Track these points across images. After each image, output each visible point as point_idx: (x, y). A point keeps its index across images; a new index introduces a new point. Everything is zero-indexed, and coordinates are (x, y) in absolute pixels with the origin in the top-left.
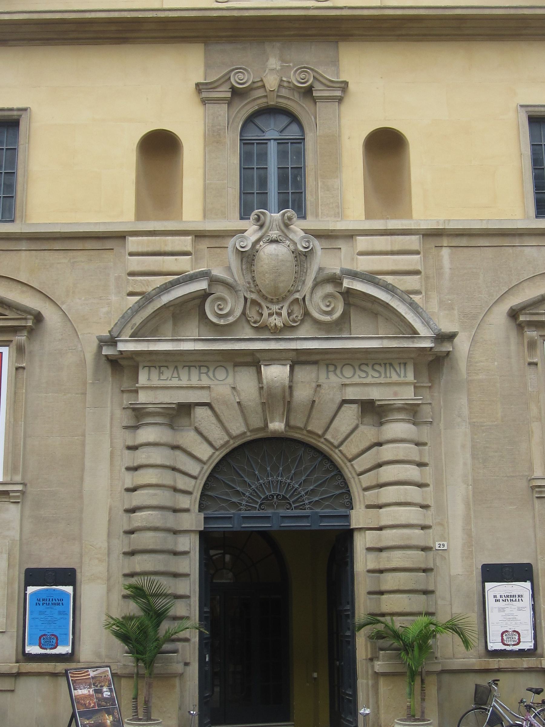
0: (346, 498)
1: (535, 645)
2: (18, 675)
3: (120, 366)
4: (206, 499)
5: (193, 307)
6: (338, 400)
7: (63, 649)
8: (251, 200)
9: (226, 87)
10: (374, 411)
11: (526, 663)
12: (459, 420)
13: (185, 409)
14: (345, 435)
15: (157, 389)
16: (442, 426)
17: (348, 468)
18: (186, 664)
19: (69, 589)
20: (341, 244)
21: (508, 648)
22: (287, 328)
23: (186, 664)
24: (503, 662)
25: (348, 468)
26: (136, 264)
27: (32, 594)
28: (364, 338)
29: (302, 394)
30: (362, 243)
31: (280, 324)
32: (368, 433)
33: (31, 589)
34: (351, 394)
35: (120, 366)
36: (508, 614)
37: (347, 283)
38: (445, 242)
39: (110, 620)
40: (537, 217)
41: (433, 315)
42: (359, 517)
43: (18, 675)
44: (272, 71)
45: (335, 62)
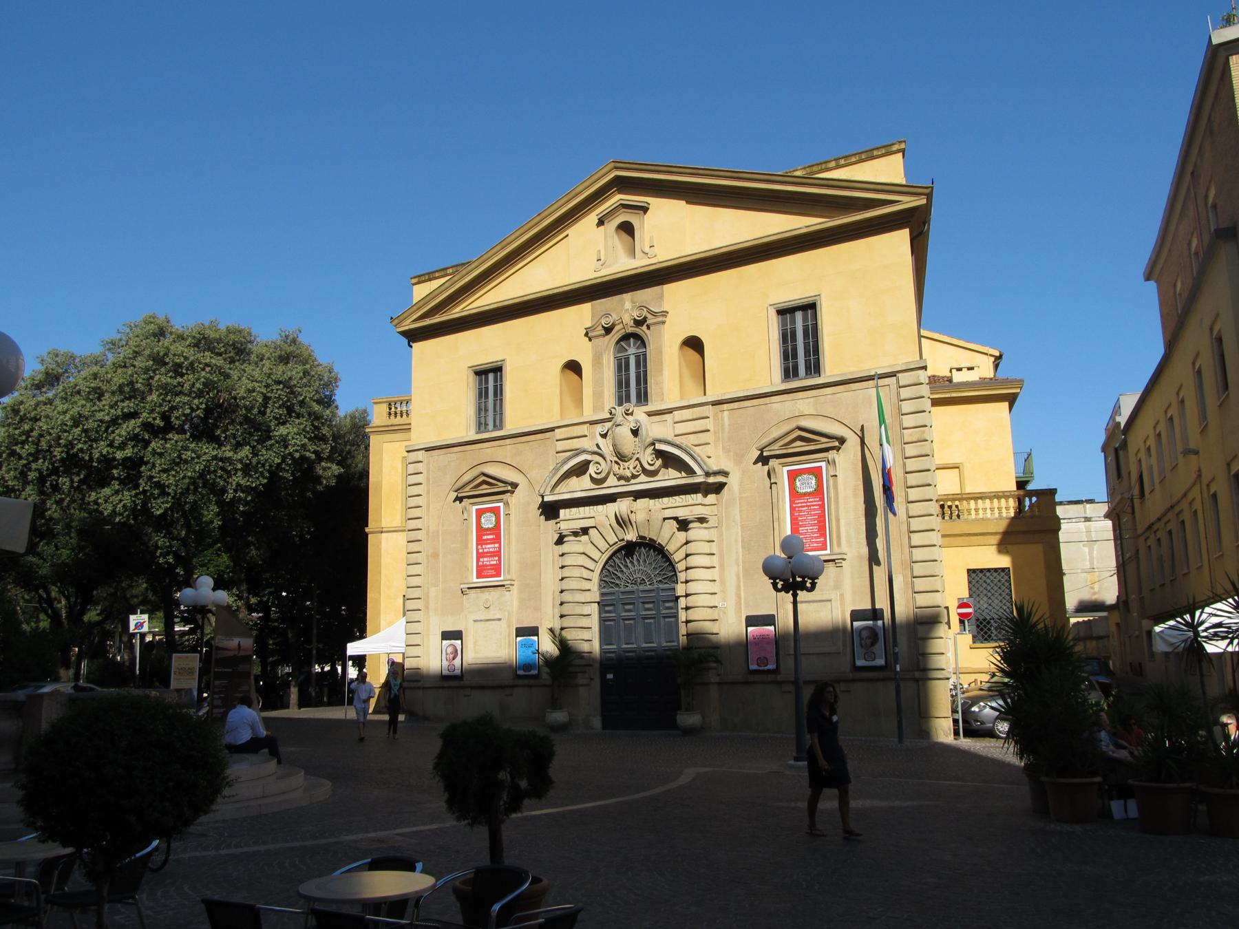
0: (674, 578)
2: (513, 686)
3: (550, 510)
4: (604, 582)
5: (581, 469)
7: (771, 667)
8: (623, 398)
10: (683, 525)
11: (770, 677)
15: (570, 518)
19: (535, 638)
20: (667, 417)
22: (634, 477)
24: (757, 678)
26: (561, 446)
28: (671, 477)
30: (678, 415)
32: (682, 536)
34: (668, 513)
37: (659, 446)
38: (725, 406)
40: (365, 411)
41: (712, 456)
42: (680, 589)
43: (854, 680)
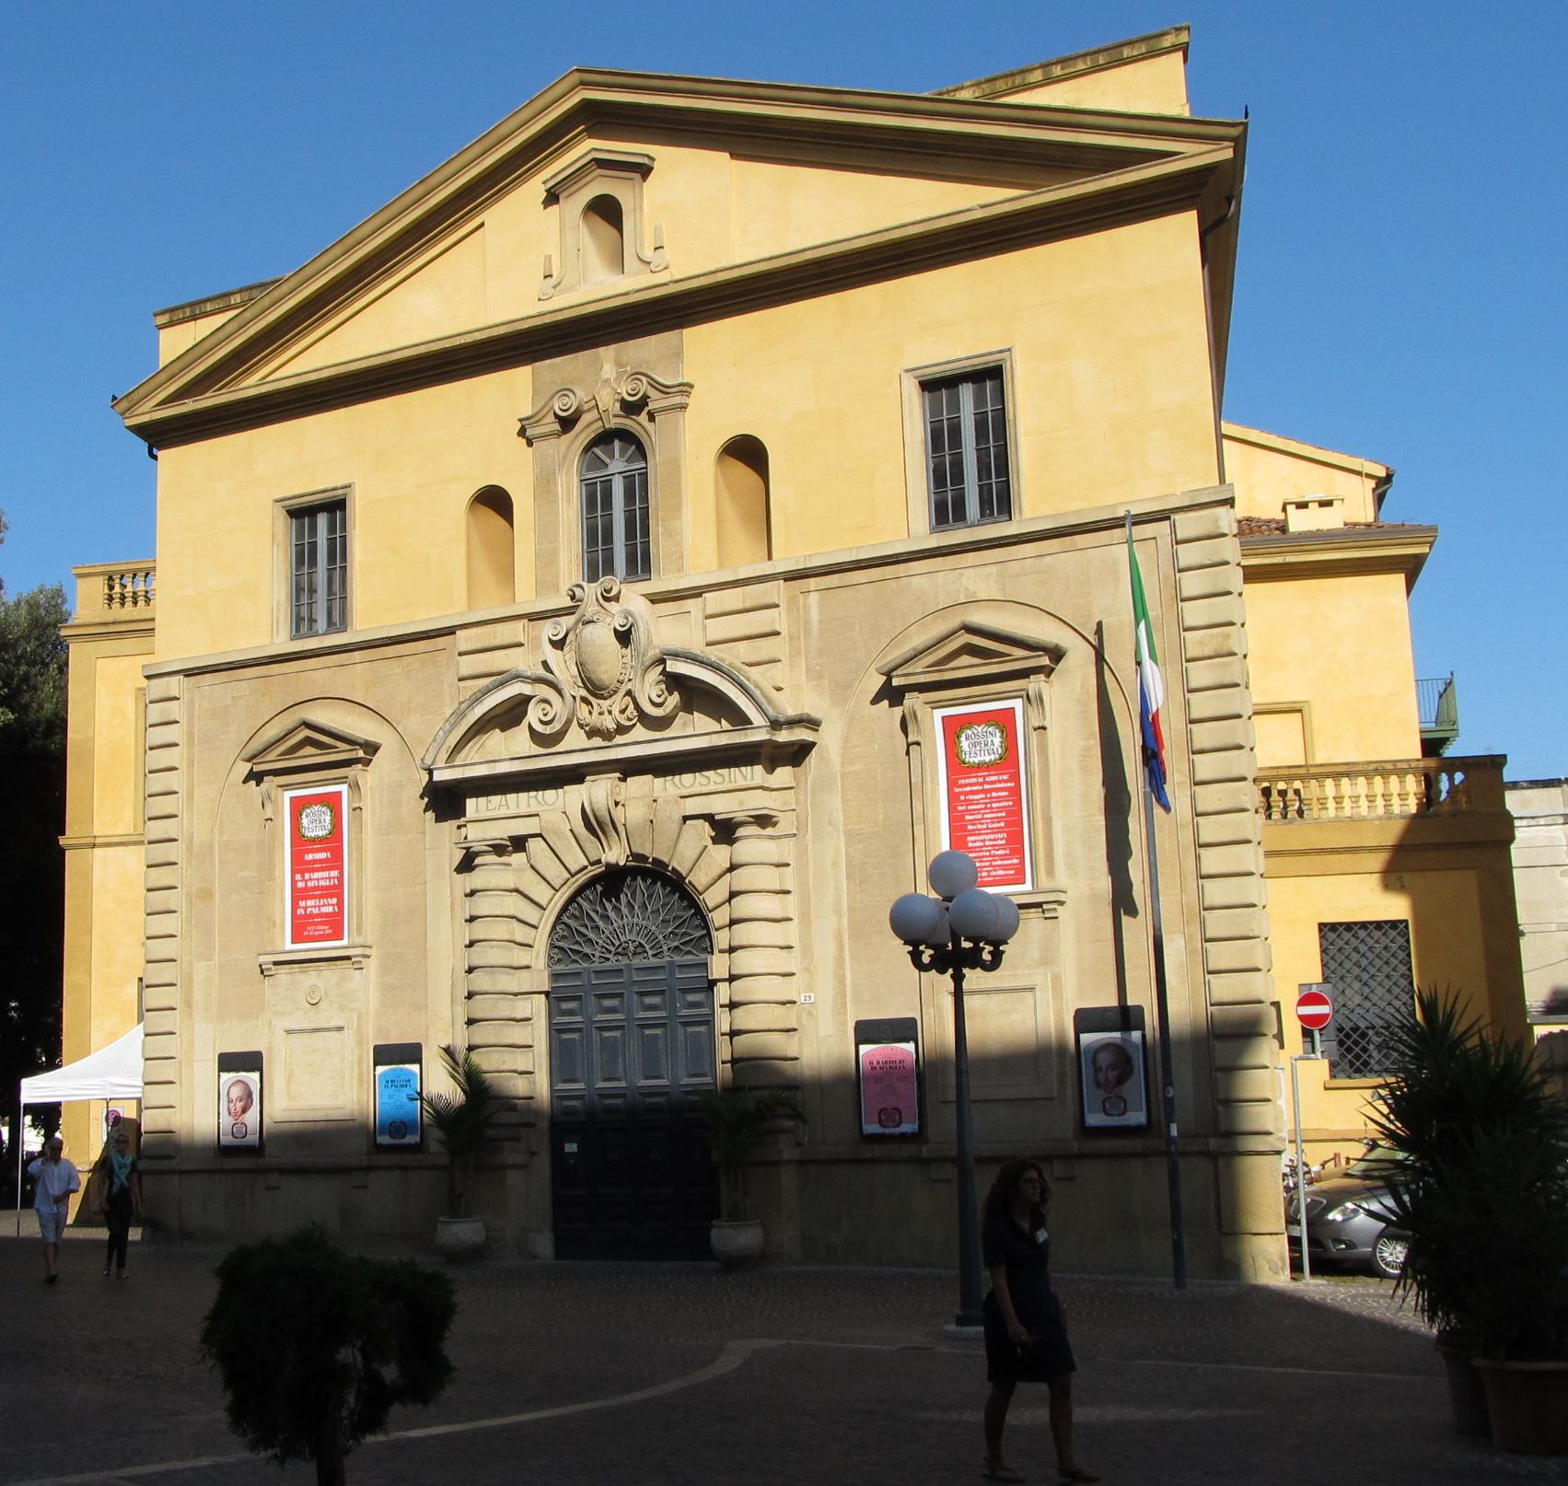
0: (704, 942)
1: (920, 1127)
2: (369, 1169)
3: (446, 800)
4: (558, 951)
5: (510, 714)
6: (677, 817)
9: (551, 418)
11: (908, 1150)
12: (829, 829)
13: (519, 843)
14: (695, 857)
16: (809, 837)
17: (837, 888)
18: (533, 1154)
19: (415, 1068)
20: (690, 604)
21: (887, 1131)
22: (622, 730)
23: (533, 1154)
25: (837, 888)
26: (469, 665)
27: (382, 1075)
28: (699, 731)
29: (633, 814)
30: (714, 601)
31: (612, 726)
32: (721, 854)
33: (380, 1069)
34: (693, 806)
35: (446, 800)
36: (1554, 1088)
39: (910, 1105)
41: (785, 686)
44: (602, 377)
45: (678, 354)
